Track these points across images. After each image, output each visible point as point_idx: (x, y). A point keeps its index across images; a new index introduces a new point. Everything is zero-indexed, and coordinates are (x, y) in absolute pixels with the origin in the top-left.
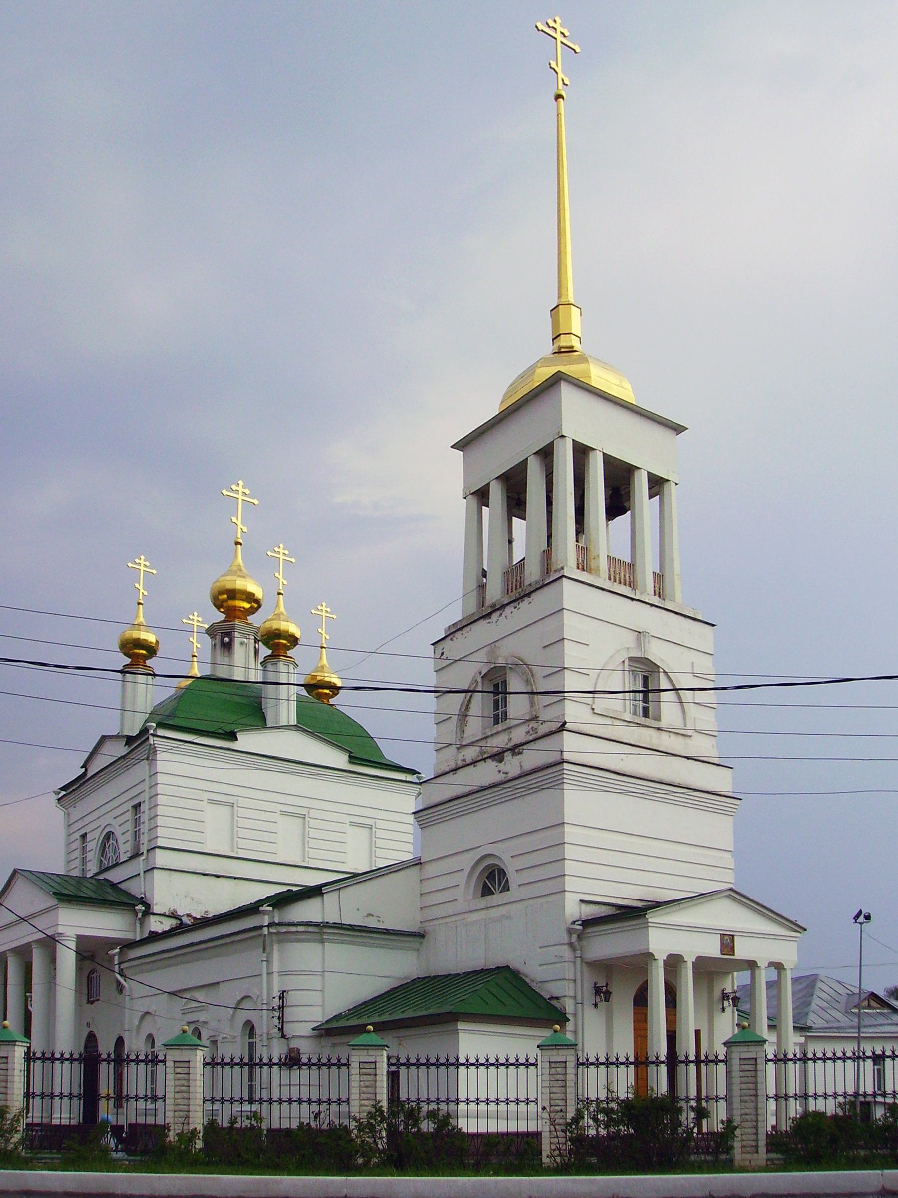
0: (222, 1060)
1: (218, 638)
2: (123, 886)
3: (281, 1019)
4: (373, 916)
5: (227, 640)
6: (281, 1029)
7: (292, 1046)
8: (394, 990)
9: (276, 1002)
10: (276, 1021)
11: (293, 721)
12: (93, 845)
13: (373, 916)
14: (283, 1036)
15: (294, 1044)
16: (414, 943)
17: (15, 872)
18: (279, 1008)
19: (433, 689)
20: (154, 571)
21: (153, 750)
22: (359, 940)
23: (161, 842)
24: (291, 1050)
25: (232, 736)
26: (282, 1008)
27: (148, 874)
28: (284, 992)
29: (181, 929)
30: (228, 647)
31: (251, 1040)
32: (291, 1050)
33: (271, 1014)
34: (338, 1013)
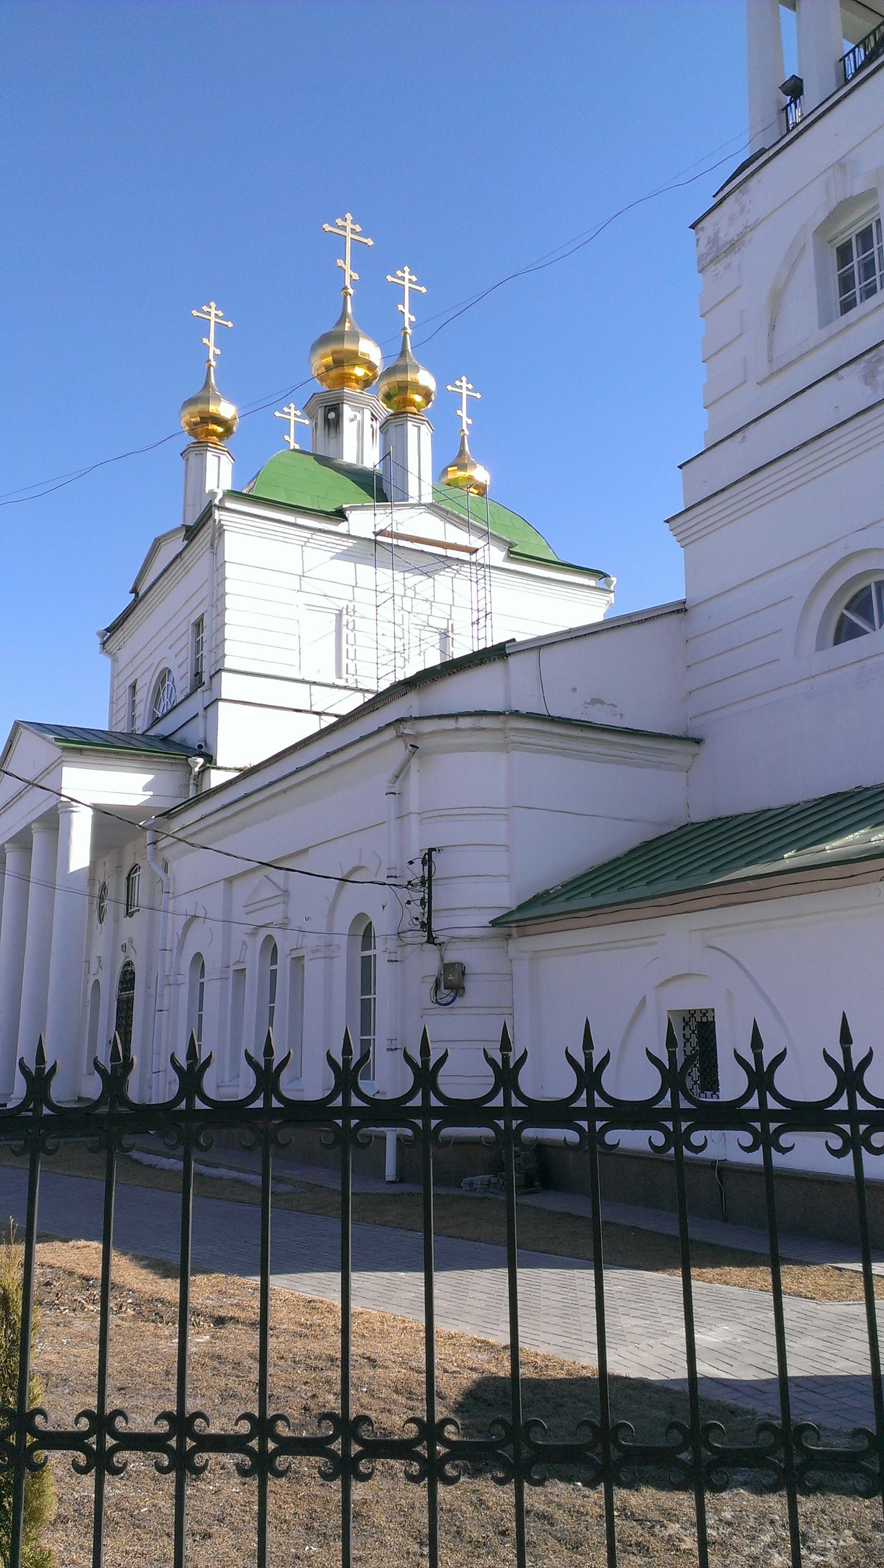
0: (589, 1077)
1: (320, 413)
2: (176, 738)
3: (427, 903)
4: (602, 703)
5: (332, 415)
6: (427, 926)
7: (450, 958)
8: (647, 846)
9: (418, 870)
10: (416, 910)
11: (428, 499)
12: (144, 695)
13: (602, 703)
14: (431, 940)
15: (451, 956)
16: (680, 754)
17: (17, 725)
18: (423, 883)
19: (456, 912)
20: (230, 324)
21: (220, 531)
22: (581, 746)
23: (228, 665)
24: (448, 967)
25: (340, 515)
26: (427, 882)
27: (210, 709)
28: (431, 850)
29: (246, 773)
30: (333, 424)
31: (367, 953)
32: (448, 967)
33: (405, 894)
34: (541, 890)
